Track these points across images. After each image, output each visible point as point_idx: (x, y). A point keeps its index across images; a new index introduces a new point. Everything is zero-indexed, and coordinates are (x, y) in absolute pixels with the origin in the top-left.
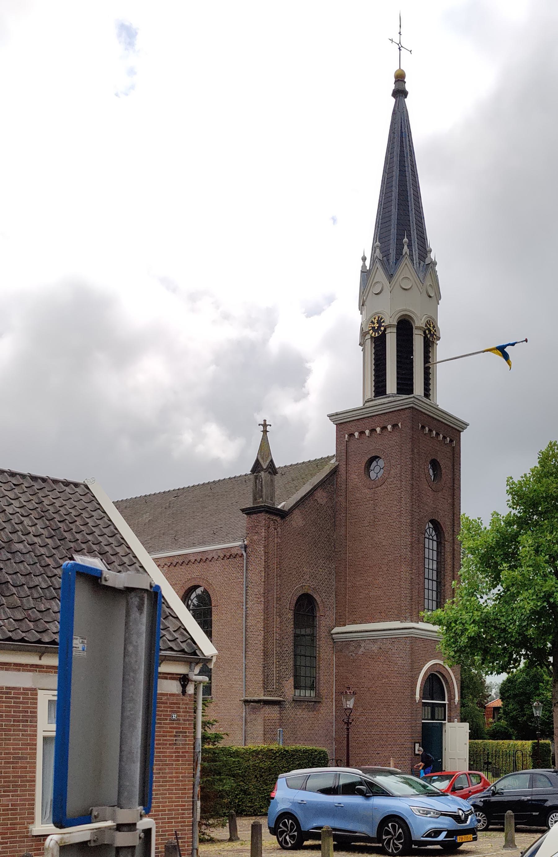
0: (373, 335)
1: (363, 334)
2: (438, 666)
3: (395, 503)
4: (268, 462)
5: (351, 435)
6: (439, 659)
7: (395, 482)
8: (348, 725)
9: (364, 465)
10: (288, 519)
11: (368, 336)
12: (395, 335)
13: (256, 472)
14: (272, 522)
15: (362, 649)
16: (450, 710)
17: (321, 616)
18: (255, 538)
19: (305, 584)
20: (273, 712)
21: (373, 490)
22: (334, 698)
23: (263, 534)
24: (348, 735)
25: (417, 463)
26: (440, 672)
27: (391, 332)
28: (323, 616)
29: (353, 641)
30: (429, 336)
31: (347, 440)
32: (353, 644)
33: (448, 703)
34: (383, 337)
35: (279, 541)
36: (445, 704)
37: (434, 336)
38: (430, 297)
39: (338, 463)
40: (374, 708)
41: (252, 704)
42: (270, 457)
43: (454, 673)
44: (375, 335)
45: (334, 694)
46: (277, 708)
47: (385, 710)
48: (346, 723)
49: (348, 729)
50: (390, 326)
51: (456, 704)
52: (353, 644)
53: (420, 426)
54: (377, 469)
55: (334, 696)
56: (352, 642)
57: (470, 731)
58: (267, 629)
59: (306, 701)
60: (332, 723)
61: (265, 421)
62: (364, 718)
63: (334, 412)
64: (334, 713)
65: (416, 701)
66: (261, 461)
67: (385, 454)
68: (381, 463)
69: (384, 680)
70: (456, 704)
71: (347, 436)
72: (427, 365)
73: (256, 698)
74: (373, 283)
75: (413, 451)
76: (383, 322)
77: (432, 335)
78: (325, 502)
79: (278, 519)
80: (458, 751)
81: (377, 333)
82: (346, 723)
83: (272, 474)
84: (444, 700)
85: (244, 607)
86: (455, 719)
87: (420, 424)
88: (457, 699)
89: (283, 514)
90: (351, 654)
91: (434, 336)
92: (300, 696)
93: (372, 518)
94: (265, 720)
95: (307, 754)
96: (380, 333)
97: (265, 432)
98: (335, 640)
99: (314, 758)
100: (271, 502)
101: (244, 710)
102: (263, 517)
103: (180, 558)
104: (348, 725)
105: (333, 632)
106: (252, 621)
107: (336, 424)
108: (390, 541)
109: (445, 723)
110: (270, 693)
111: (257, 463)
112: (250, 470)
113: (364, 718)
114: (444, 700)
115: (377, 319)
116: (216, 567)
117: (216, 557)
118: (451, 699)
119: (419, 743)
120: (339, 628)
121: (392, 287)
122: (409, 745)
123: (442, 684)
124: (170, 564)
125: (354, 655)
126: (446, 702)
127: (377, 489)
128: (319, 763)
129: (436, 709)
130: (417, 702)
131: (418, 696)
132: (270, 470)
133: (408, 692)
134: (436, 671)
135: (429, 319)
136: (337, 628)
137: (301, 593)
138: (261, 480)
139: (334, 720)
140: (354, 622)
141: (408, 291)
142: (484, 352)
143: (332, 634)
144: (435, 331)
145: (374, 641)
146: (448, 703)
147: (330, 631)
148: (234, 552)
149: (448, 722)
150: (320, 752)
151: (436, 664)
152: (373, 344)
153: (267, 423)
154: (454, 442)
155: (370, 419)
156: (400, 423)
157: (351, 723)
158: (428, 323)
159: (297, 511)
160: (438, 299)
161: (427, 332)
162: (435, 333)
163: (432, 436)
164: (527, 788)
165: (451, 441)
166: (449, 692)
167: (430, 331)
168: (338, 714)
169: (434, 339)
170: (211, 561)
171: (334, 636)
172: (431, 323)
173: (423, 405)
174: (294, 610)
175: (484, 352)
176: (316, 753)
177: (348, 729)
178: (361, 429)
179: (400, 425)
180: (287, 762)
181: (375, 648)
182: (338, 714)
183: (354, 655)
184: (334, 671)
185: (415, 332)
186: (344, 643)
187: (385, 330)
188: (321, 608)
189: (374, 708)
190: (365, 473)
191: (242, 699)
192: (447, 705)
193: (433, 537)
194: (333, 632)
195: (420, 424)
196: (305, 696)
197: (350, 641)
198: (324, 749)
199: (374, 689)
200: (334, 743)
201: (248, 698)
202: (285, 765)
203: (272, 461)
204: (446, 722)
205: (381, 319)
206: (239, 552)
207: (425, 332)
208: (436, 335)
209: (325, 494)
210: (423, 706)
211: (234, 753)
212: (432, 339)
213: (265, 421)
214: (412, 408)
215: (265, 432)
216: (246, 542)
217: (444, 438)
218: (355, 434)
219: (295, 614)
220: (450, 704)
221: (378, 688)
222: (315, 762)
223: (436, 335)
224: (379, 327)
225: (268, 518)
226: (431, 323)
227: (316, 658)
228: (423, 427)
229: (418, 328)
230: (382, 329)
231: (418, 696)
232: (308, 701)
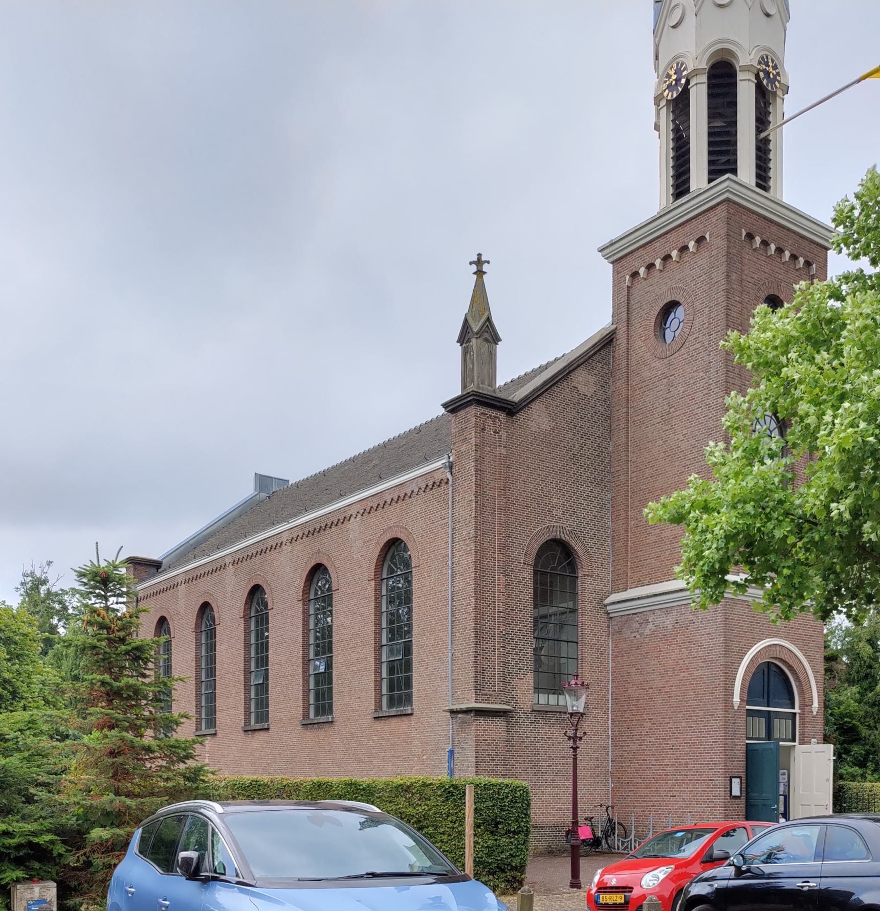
0: (669, 98)
1: (658, 99)
2: (778, 648)
3: (702, 374)
4: (482, 320)
5: (635, 275)
6: (781, 637)
7: (700, 339)
8: (575, 742)
9: (653, 320)
10: (521, 416)
11: (663, 103)
12: (704, 89)
13: (465, 341)
14: (490, 421)
15: (650, 625)
16: (803, 724)
17: (585, 575)
18: (463, 448)
19: (556, 524)
20: (496, 728)
21: (668, 359)
22: (610, 708)
23: (473, 441)
24: (575, 759)
25: (738, 299)
26: (782, 659)
27: (696, 84)
28: (588, 576)
29: (636, 614)
30: (765, 82)
31: (630, 285)
32: (637, 619)
33: (799, 711)
34: (685, 92)
35: (503, 451)
36: (795, 714)
37: (777, 83)
38: (768, 15)
39: (615, 326)
40: (667, 720)
41: (460, 716)
42: (487, 313)
43: (810, 662)
44: (672, 95)
45: (610, 701)
46: (501, 722)
47: (684, 724)
48: (570, 738)
49: (575, 749)
50: (696, 72)
51: (815, 713)
52: (637, 619)
53: (744, 233)
54: (675, 323)
55: (610, 706)
56: (635, 616)
57: (835, 758)
58: (480, 593)
59: (557, 712)
60: (605, 748)
61: (479, 255)
62: (653, 739)
63: (606, 241)
64: (610, 733)
65: (733, 706)
66: (470, 321)
67: (685, 294)
68: (680, 312)
69: (683, 674)
70: (815, 713)
71: (628, 277)
72: (763, 135)
73: (464, 706)
74: (672, 6)
75: (728, 276)
76: (685, 69)
77: (773, 81)
78: (592, 391)
79: (502, 416)
80: (816, 793)
81: (675, 92)
82: (570, 738)
83: (490, 342)
84: (794, 708)
85: (450, 562)
86: (813, 740)
87: (743, 230)
88: (816, 705)
89: (510, 409)
90: (633, 635)
91: (777, 83)
92: (538, 704)
93: (666, 407)
94: (477, 742)
95: (491, 791)
96: (680, 89)
97: (480, 273)
98: (611, 615)
99: (502, 799)
100: (490, 388)
101: (451, 726)
102: (472, 411)
103: (375, 499)
104: (575, 742)
105: (606, 601)
106: (460, 585)
107: (613, 263)
108: (692, 442)
109: (795, 746)
110: (487, 698)
111: (466, 325)
112: (456, 339)
113: (653, 739)
114: (794, 708)
115: (675, 68)
116: (416, 506)
117: (416, 490)
118: (806, 705)
119: (740, 777)
120: (616, 594)
121: (697, 8)
122: (721, 781)
123: (790, 682)
124: (363, 511)
125: (638, 636)
126: (797, 710)
127: (673, 356)
128: (512, 807)
129: (776, 721)
130: (736, 708)
131: (736, 699)
132: (486, 335)
133: (720, 693)
134: (776, 658)
135: (767, 53)
136: (613, 595)
137: (547, 537)
138: (472, 353)
139: (610, 743)
140: (640, 584)
141: (727, 9)
142: (859, 81)
143: (606, 606)
144: (778, 74)
145: (668, 611)
146: (799, 711)
147: (602, 600)
148: (438, 477)
149: (800, 744)
150: (515, 789)
151: (775, 645)
152: (671, 114)
153: (483, 259)
154: (814, 266)
155: (662, 240)
156: (708, 233)
157: (581, 738)
158: (763, 60)
159: (536, 406)
160: (785, 21)
161: (762, 75)
162: (778, 78)
163: (769, 254)
164: (810, 861)
165: (808, 264)
166: (802, 693)
167: (767, 74)
168: (616, 734)
169: (776, 87)
170: (410, 497)
171: (609, 608)
172: (770, 61)
173: (755, 199)
174: (535, 566)
175: (859, 81)
176: (507, 791)
177: (575, 749)
178: (648, 261)
179: (707, 236)
180: (455, 805)
181: (669, 623)
182: (616, 734)
183: (638, 636)
184: (610, 665)
185: (740, 76)
186: (624, 619)
187: (688, 82)
188: (584, 563)
189: (667, 720)
190: (655, 335)
191: (447, 708)
192: (798, 717)
193: (771, 432)
194: (606, 601)
195: (743, 230)
196: (548, 704)
197: (633, 614)
198: (524, 783)
199: (667, 689)
200: (610, 779)
201: (454, 707)
202: (451, 811)
203: (489, 319)
204: (796, 743)
205: (682, 64)
206: (443, 477)
207: (757, 76)
208: (779, 82)
209: (592, 379)
210: (747, 716)
211: (364, 789)
212: (772, 88)
213: (479, 255)
214: (728, 200)
215: (480, 273)
216: (451, 459)
217: (794, 257)
218: (640, 272)
219: (535, 572)
220: (802, 715)
221: (674, 688)
222: (505, 806)
223: (779, 82)
224: (678, 81)
225: (482, 413)
226: (770, 61)
227: (577, 643)
228: (750, 236)
229: (746, 69)
230: (683, 81)
231: (736, 699)
232: (560, 712)
